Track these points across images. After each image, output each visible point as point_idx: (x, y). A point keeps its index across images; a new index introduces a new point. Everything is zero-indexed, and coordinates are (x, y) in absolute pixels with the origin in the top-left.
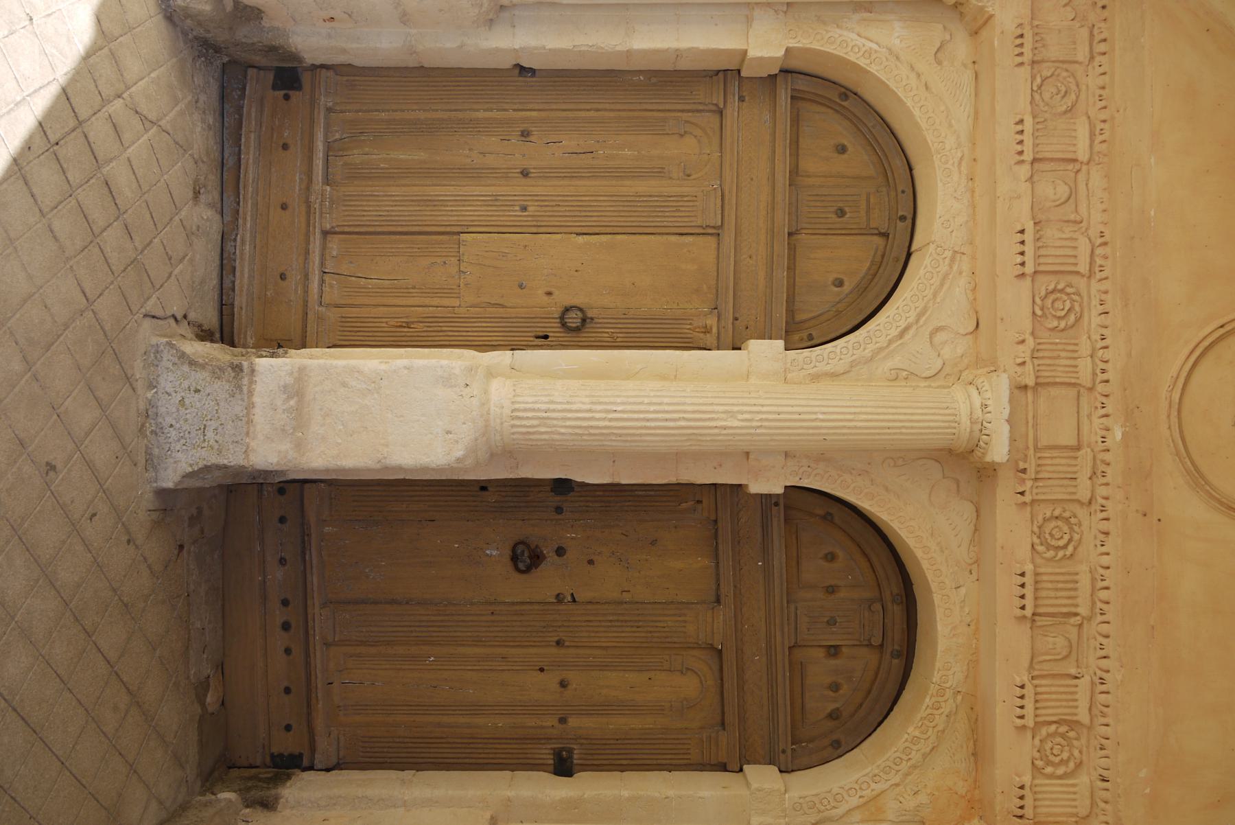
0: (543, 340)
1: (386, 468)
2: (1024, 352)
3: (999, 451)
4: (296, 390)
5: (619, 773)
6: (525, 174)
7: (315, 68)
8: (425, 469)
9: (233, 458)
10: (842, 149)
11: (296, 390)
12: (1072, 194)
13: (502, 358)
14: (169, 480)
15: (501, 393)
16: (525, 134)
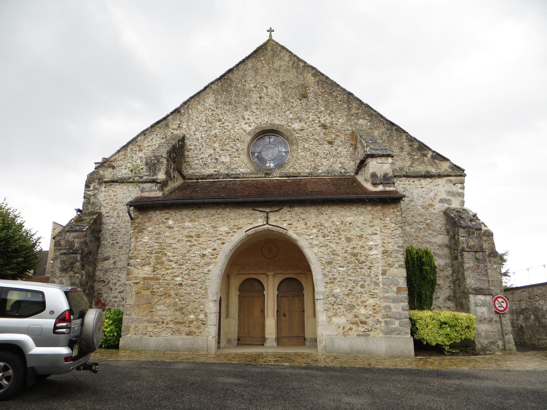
9: (274, 339)
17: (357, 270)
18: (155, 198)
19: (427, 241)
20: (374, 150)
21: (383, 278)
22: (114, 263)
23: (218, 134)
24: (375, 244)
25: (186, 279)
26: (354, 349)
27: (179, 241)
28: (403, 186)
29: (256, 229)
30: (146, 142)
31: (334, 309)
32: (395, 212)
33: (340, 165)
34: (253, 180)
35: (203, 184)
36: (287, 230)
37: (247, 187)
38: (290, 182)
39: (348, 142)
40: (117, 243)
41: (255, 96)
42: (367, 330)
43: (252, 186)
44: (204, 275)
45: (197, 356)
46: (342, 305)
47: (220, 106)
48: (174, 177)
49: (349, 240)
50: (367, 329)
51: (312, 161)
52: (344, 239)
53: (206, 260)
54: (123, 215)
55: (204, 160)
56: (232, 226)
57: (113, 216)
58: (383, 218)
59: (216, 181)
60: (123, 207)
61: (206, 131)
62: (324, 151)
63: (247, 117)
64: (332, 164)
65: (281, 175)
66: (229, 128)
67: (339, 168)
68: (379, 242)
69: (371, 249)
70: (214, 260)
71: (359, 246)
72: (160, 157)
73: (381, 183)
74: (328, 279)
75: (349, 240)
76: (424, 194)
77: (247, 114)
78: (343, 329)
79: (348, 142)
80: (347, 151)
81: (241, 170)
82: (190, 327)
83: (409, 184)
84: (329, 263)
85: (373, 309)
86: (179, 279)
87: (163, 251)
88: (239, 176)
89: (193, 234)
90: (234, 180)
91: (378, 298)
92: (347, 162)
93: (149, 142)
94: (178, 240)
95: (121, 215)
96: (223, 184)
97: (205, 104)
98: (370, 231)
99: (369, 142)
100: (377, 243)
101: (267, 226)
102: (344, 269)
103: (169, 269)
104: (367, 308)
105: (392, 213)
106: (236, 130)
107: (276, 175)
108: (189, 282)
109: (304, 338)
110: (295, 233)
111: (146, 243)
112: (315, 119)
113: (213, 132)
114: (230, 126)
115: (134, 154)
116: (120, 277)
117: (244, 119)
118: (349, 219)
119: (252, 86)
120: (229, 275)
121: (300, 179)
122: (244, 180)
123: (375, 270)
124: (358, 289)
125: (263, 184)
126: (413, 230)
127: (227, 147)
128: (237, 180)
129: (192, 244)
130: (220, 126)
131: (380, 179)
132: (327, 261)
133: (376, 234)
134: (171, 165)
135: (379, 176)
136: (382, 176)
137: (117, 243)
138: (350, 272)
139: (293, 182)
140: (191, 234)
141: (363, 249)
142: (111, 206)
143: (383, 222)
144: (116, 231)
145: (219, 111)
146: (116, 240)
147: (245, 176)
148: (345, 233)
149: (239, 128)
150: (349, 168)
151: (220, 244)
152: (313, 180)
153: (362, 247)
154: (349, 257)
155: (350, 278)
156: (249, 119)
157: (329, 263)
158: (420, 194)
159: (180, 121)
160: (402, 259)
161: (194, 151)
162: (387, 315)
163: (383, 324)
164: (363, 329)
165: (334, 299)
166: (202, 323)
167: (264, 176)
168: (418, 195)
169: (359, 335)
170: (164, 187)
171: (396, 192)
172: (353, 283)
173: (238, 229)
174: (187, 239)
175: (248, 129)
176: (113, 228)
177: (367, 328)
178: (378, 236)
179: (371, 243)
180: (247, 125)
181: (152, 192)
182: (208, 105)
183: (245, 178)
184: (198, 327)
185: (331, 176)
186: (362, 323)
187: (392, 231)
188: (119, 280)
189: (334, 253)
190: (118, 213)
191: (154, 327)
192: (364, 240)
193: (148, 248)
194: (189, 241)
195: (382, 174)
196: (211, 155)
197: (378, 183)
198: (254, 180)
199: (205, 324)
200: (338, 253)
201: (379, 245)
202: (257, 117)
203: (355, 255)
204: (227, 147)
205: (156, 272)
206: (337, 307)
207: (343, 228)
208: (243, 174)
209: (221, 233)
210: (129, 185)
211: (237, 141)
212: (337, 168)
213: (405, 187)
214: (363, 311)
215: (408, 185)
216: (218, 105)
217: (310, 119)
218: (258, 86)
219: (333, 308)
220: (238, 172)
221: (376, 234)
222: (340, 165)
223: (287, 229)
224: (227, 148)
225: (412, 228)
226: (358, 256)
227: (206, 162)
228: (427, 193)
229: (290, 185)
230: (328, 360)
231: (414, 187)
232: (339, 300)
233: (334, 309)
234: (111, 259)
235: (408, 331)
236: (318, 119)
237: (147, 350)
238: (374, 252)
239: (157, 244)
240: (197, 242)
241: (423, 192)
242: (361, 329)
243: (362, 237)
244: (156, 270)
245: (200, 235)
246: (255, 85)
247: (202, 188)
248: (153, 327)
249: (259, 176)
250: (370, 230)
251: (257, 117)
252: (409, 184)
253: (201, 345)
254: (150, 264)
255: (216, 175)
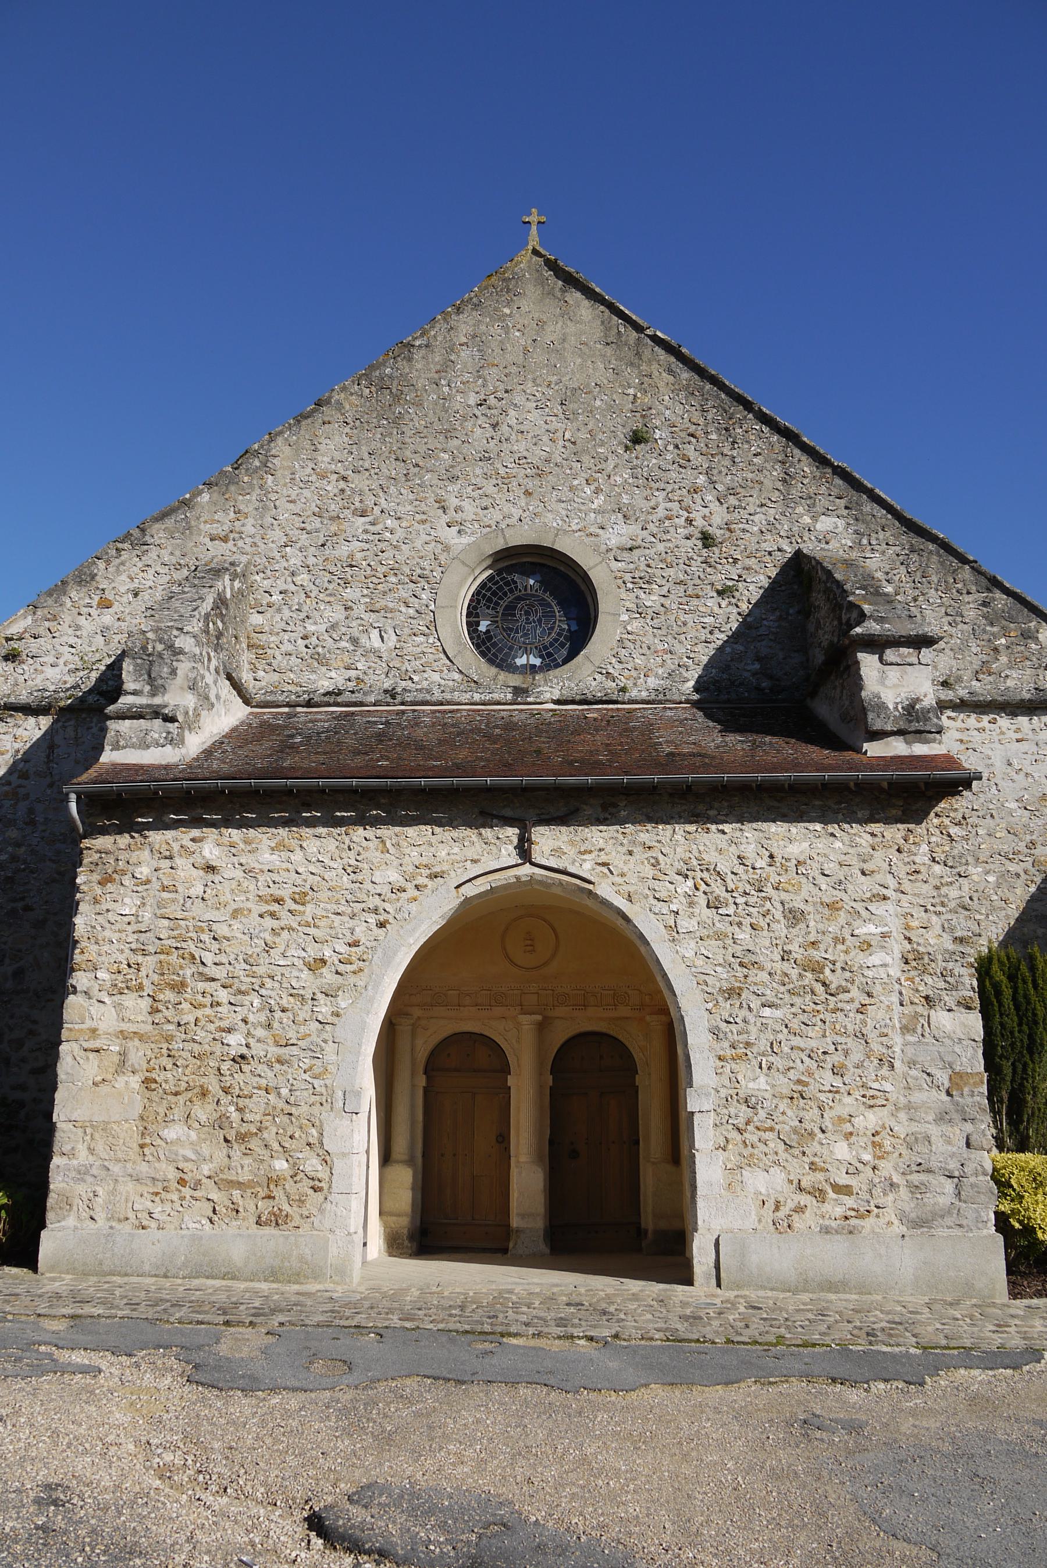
0: (507, 1149)
1: (545, 1190)
2: (512, 1009)
3: (539, 1018)
4: (523, 1216)
5: (57, 1134)
6: (454, 1155)
7: (421, 1223)
8: (545, 1180)
9: (542, 1233)
10: (449, 1055)
11: (523, 1216)
12: (468, 995)
13: (513, 1160)
14: (547, 1251)
15: (523, 1159)
16: (442, 1155)
17: (822, 1016)
18: (160, 767)
19: (1036, 916)
20: (875, 620)
21: (906, 1044)
22: (18, 974)
23: (359, 556)
24: (879, 930)
25: (259, 1041)
26: (811, 1274)
27: (236, 913)
28: (958, 735)
29: (490, 877)
30: (124, 577)
31: (746, 1145)
32: (946, 827)
33: (757, 666)
34: (474, 711)
35: (311, 721)
36: (593, 883)
37: (459, 734)
38: (595, 719)
39: (783, 588)
40: (27, 908)
41: (479, 434)
42: (853, 1213)
43: (472, 731)
44: (320, 1026)
45: (301, 1298)
46: (772, 1129)
47: (367, 465)
48: (218, 697)
49: (795, 917)
50: (854, 1210)
51: (665, 651)
52: (778, 915)
53: (327, 975)
54: (46, 819)
55: (314, 640)
56: (411, 868)
57: (15, 820)
58: (906, 847)
59: (353, 713)
60: (49, 792)
61: (323, 545)
62: (706, 620)
63: (453, 502)
64: (732, 660)
65: (567, 694)
66: (394, 539)
67: (754, 674)
68: (895, 926)
69: (866, 946)
70: (352, 979)
71: (828, 939)
72: (175, 632)
73: (900, 733)
74: (726, 1044)
75: (795, 917)
76: (1028, 762)
77: (451, 495)
78: (777, 1208)
79: (783, 588)
80: (780, 618)
81: (436, 677)
82: (274, 1198)
83: (978, 730)
84: (732, 993)
85: (873, 1142)
86: (233, 1039)
87: (184, 945)
88: (429, 698)
89: (285, 893)
90: (414, 711)
91: (890, 1107)
92: (781, 655)
93: (132, 579)
94: (236, 911)
95: (40, 819)
96: (375, 723)
97: (320, 458)
98: (436, 677)
99: (857, 592)
100: (886, 929)
101: (526, 870)
102: (778, 1013)
103: (202, 1006)
104: (853, 1139)
105: (937, 830)
106: (418, 544)
107: (548, 696)
108: (274, 1051)
109: (639, 1229)
110: (618, 892)
111: (126, 919)
112: (674, 513)
113: (343, 550)
114: (400, 534)
115: (83, 617)
116: (35, 1022)
117: (444, 509)
118: (796, 850)
119: (473, 400)
120: (394, 1021)
121: (629, 711)
122: (445, 711)
123: (881, 1014)
124: (828, 1079)
125: (509, 726)
126: (991, 879)
127: (389, 602)
128: (424, 711)
129: (282, 923)
130: (366, 531)
131: (895, 716)
132: (725, 985)
133: (885, 898)
134: (209, 660)
135: (891, 707)
136: (900, 707)
137: (27, 908)
138: (795, 1025)
139: (609, 721)
140: (278, 893)
141: (840, 947)
142: (6, 788)
143: (907, 860)
144: (24, 870)
145: (359, 482)
146: (23, 899)
147: (448, 696)
148: (784, 896)
149: (428, 538)
150: (785, 674)
151: (374, 927)
152: (669, 713)
153: (838, 940)
154: (794, 973)
155: (797, 1041)
156: (458, 509)
157: (732, 993)
158: (1015, 762)
159: (235, 512)
160: (967, 980)
161: (279, 610)
162: (920, 1164)
163: (904, 1192)
164: (839, 1211)
165: (744, 1112)
166: (312, 1188)
167: (509, 696)
168: (1010, 764)
169: (826, 1230)
170: (187, 733)
171: (949, 761)
172: (806, 1059)
173: (434, 876)
174: (265, 908)
175: (459, 542)
176: (14, 858)
177: (855, 1206)
178: (889, 906)
179: (871, 928)
180: (454, 529)
181: (148, 747)
182: (326, 459)
183: (449, 703)
184: (300, 1200)
185: (728, 701)
186: (838, 1189)
187: (937, 888)
188: (31, 1032)
189: (747, 962)
190: (31, 811)
191: (154, 1198)
192: (842, 917)
193: (135, 936)
194: (273, 915)
195: (899, 700)
196: (334, 627)
197: (889, 728)
198: (479, 710)
199: (321, 1189)
200: (760, 958)
201: (894, 934)
202: (486, 502)
203: (816, 968)
204: (389, 602)
205: (160, 1015)
206: (755, 1139)
207: (774, 879)
208: (443, 692)
209: (378, 892)
210: (69, 720)
211: (423, 583)
212: (746, 674)
213: (965, 739)
214: (842, 1151)
215: (976, 733)
216: (361, 462)
217: (661, 512)
218: (492, 401)
219: (744, 1142)
220: (425, 684)
221: (885, 898)
222: (757, 666)
223: (592, 879)
224: (391, 605)
225: (987, 873)
226: (827, 971)
227: (320, 650)
228: (1037, 757)
229: (597, 730)
230: (731, 1317)
231: (996, 739)
232: (762, 1114)
233: (746, 1145)
234: (7, 961)
235: (988, 1215)
236: (686, 514)
237: (129, 1271)
238: (876, 959)
239: (166, 922)
240: (298, 919)
241: (1025, 756)
242: (835, 1207)
243: (838, 910)
244: (160, 1007)
245: (305, 894)
246: (483, 397)
247: (309, 738)
248: (149, 1197)
249: (496, 696)
250: (865, 886)
251: (486, 502)
252: (978, 730)
253: (310, 1257)
254: (141, 987)
255: (353, 692)
